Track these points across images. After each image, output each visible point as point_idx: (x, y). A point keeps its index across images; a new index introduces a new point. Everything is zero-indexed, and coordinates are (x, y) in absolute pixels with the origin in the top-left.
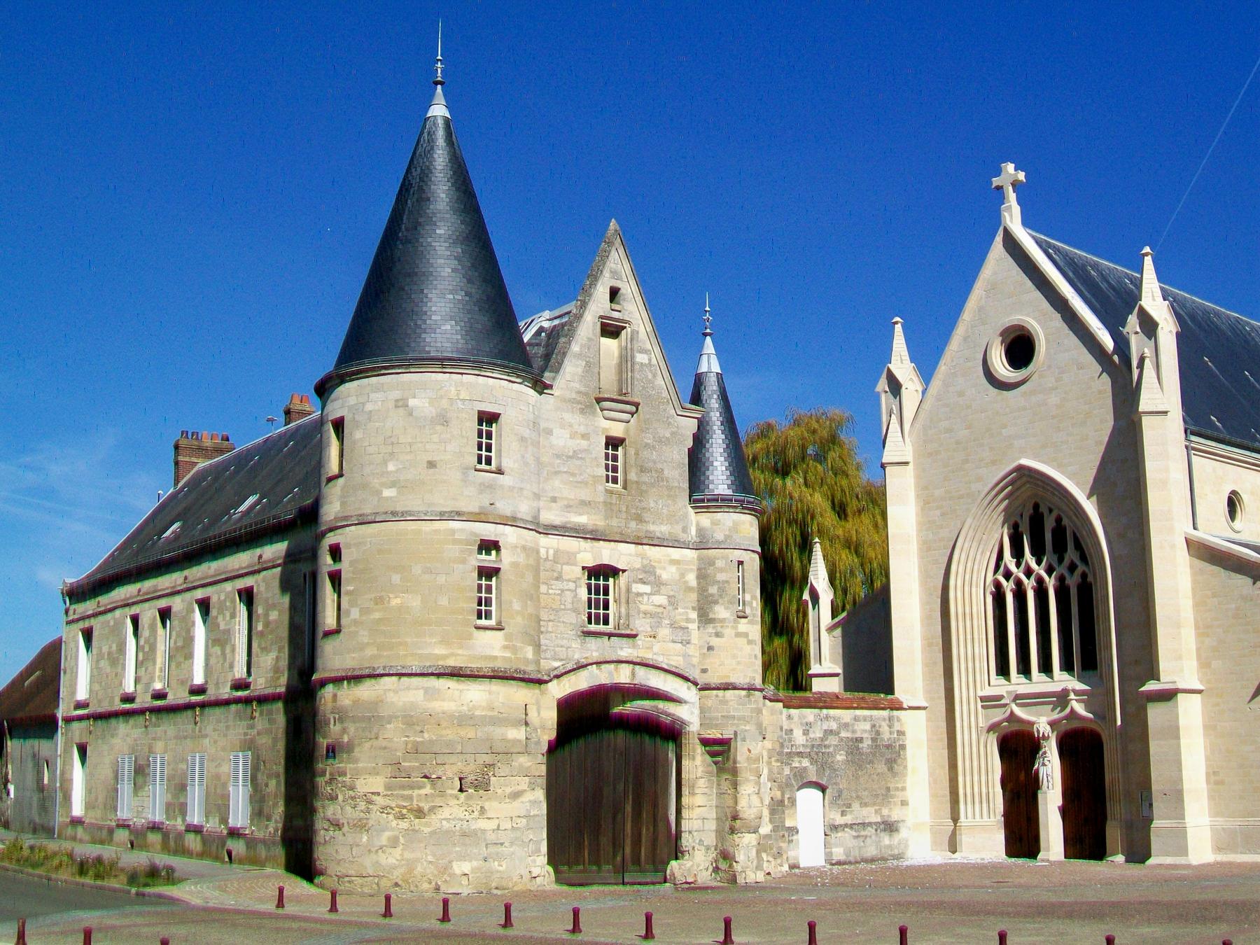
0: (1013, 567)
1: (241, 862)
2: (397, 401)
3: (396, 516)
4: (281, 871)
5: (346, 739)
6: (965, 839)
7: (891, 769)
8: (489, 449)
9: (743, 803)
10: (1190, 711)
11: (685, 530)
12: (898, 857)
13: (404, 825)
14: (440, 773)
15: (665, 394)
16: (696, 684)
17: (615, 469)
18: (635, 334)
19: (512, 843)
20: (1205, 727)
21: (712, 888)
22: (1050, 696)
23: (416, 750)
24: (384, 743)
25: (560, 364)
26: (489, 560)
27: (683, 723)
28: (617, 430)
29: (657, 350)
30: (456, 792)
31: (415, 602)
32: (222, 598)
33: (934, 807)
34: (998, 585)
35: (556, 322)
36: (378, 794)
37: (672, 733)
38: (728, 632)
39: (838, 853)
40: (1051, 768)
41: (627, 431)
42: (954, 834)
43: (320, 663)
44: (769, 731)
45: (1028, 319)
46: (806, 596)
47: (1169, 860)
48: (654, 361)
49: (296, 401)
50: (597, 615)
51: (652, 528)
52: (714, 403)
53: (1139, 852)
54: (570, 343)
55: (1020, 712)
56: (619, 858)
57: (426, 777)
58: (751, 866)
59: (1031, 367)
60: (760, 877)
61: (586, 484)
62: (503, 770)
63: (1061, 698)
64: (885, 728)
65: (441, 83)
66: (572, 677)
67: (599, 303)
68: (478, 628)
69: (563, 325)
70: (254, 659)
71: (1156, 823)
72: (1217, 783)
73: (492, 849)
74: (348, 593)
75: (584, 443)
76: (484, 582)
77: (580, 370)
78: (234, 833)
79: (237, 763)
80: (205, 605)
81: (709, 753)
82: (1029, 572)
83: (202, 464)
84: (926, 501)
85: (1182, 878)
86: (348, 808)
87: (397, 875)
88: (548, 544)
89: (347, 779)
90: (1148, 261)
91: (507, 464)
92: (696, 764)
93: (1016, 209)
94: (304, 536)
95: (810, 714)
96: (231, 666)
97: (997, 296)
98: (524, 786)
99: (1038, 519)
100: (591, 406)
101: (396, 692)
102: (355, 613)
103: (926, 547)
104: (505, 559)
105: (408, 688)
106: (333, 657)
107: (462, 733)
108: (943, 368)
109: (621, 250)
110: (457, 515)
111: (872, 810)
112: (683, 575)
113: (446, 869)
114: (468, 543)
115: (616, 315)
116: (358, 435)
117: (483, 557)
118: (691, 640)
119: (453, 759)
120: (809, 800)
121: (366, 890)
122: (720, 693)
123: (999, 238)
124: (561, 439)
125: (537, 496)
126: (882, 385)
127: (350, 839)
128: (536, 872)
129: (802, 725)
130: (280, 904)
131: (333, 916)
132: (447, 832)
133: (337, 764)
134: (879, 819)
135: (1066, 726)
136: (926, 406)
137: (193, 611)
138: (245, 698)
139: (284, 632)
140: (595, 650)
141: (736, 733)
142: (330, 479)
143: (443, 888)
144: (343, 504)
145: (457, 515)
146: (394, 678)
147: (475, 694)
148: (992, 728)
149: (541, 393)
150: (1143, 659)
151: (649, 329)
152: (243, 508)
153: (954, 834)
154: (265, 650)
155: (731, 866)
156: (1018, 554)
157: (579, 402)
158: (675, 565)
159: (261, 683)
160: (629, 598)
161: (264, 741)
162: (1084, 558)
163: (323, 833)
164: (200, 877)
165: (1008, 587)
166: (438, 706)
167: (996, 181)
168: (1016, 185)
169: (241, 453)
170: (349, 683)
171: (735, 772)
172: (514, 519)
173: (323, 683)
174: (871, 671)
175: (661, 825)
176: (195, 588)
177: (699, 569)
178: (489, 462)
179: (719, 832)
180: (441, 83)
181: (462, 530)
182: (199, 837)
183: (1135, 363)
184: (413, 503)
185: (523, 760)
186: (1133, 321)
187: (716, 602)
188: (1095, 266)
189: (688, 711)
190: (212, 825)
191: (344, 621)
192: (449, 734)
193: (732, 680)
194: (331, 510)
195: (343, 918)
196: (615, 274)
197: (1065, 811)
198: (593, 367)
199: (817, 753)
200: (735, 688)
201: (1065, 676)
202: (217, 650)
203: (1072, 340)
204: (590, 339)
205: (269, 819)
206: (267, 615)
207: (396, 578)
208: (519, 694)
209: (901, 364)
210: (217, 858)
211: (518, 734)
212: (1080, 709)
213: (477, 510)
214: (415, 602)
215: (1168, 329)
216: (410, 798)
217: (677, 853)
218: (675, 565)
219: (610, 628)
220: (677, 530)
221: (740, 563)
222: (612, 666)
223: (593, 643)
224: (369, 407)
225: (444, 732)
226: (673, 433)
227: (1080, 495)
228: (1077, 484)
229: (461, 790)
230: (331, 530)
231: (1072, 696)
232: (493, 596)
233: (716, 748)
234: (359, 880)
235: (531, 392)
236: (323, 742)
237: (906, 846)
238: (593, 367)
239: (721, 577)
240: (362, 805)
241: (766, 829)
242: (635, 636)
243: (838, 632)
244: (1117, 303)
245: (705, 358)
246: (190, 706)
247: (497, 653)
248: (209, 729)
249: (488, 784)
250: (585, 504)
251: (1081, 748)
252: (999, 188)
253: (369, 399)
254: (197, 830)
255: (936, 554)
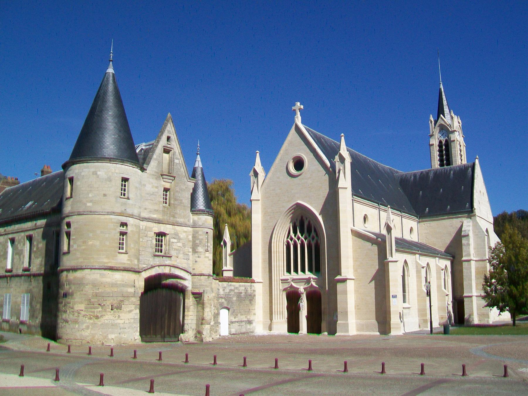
0: (293, 236)
1: (25, 333)
2: (93, 172)
3: (91, 213)
4: (41, 337)
5: (71, 291)
6: (274, 326)
7: (250, 303)
8: (125, 190)
9: (206, 315)
10: (350, 286)
11: (189, 221)
12: (252, 332)
13: (91, 321)
14: (105, 303)
15: (184, 174)
16: (191, 273)
17: (166, 199)
18: (174, 154)
19: (129, 328)
20: (355, 291)
21: (196, 343)
22: (304, 280)
23: (96, 295)
24: (85, 293)
25: (150, 162)
26: (124, 229)
27: (186, 287)
28: (168, 186)
29: (182, 159)
30: (110, 310)
31: (97, 243)
32: (20, 238)
33: (265, 317)
34: (288, 242)
35: (148, 147)
36: (82, 310)
37: (182, 290)
38: (202, 256)
39: (233, 331)
40: (304, 304)
41: (171, 186)
42: (271, 325)
43: (61, 264)
44: (213, 289)
45: (304, 156)
46: (222, 243)
47: (342, 334)
48: (181, 163)
49: (46, 168)
50: (158, 249)
51: (178, 220)
52: (200, 178)
53: (332, 331)
54: (153, 155)
55: (294, 285)
56: (163, 333)
57: (99, 305)
58: (207, 337)
59: (303, 170)
60: (211, 340)
61: (156, 204)
62: (126, 302)
63: (308, 280)
64: (249, 289)
65: (112, 61)
66: (150, 271)
67: (163, 142)
68: (119, 253)
69: (150, 149)
70: (32, 260)
71: (339, 322)
72: (358, 309)
73: (122, 330)
74: (73, 239)
75: (156, 190)
76: (121, 237)
77: (156, 164)
78: (22, 323)
79: (24, 298)
80: (13, 241)
81: (195, 298)
82: (299, 238)
83: (8, 188)
84: (265, 213)
85: (349, 340)
86: (71, 316)
87: (88, 339)
88: (143, 224)
89: (71, 305)
90: (343, 138)
91: (131, 196)
92: (190, 301)
93: (300, 118)
94: (54, 218)
95: (225, 284)
96: (23, 263)
97: (292, 146)
98: (133, 308)
99: (302, 221)
100: (159, 177)
101: (90, 274)
102: (75, 246)
103: (264, 229)
104: (129, 229)
105: (94, 274)
106: (66, 262)
107: (113, 290)
108: (273, 169)
109: (172, 124)
110: (113, 213)
111: (244, 316)
112: (187, 236)
113: (106, 337)
114: (117, 223)
115: (169, 146)
116: (78, 183)
117: (122, 228)
118: (190, 259)
119: (110, 298)
120: (224, 313)
121: (77, 344)
122: (199, 277)
123: (294, 127)
124: (149, 188)
125: (140, 207)
126: (252, 173)
127: (71, 326)
128: (136, 338)
129: (222, 288)
130: (48, 349)
131: (69, 354)
132: (107, 324)
133: (68, 300)
134: (246, 320)
135: (309, 290)
136: (266, 181)
137: (8, 242)
138: (28, 275)
139: (44, 251)
140: (158, 261)
141: (204, 291)
142: (67, 199)
143: (105, 344)
144: (72, 208)
145: (113, 213)
146: (89, 270)
147: (118, 276)
148: (284, 290)
149: (143, 172)
150: (336, 268)
151: (180, 151)
152: (28, 205)
153: (271, 325)
154: (37, 258)
155: (201, 336)
156: (295, 232)
157: (155, 175)
158: (185, 233)
159: (34, 269)
160: (170, 244)
161: (35, 290)
162: (317, 235)
163: (61, 324)
164: (14, 339)
165: (292, 243)
166: (105, 280)
167: (293, 108)
168: (300, 110)
169: (23, 186)
170: (72, 271)
171: (203, 304)
172: (133, 215)
173: (62, 271)
174: (243, 269)
175: (177, 322)
176: (9, 234)
177: (193, 234)
178: (124, 195)
179: (197, 325)
180: (112, 61)
181: (115, 219)
182: (8, 325)
183: (337, 171)
184: (97, 208)
185: (133, 299)
186: (337, 157)
187: (198, 246)
188: (323, 138)
189: (188, 283)
190: (14, 320)
191: (71, 249)
192: (108, 290)
193: (203, 273)
194: (68, 208)
195: (219, 367)
196: (169, 132)
197: (308, 318)
198: (160, 163)
199: (227, 297)
200: (204, 275)
201: (309, 273)
202: (17, 257)
203: (316, 162)
204: (160, 154)
205: (37, 318)
206: (38, 245)
207: (91, 235)
208: (131, 276)
209: (258, 167)
210: (15, 332)
211: (131, 290)
212: (314, 284)
213: (120, 212)
214: (97, 243)
215: (348, 161)
216: (94, 312)
217: (183, 331)
218: (185, 233)
219: (162, 254)
220: (186, 221)
221: (207, 233)
222: (163, 267)
223: (157, 259)
224: (83, 174)
225: (107, 289)
226: (186, 188)
227: (317, 214)
228: (316, 210)
229: (112, 309)
230: (67, 216)
231: (312, 280)
232: (124, 242)
233: (197, 296)
234: (74, 341)
235: (140, 171)
236: (62, 292)
237: (255, 329)
238: (160, 163)
239: (200, 237)
240: (76, 314)
241: (212, 323)
242: (171, 257)
243: (232, 256)
244: (332, 152)
245: (197, 162)
246: (5, 277)
247: (125, 262)
248: (13, 285)
249: (121, 307)
250: (156, 211)
251: (314, 298)
252: (294, 110)
253: (81, 171)
254: (7, 321)
255: (268, 231)
